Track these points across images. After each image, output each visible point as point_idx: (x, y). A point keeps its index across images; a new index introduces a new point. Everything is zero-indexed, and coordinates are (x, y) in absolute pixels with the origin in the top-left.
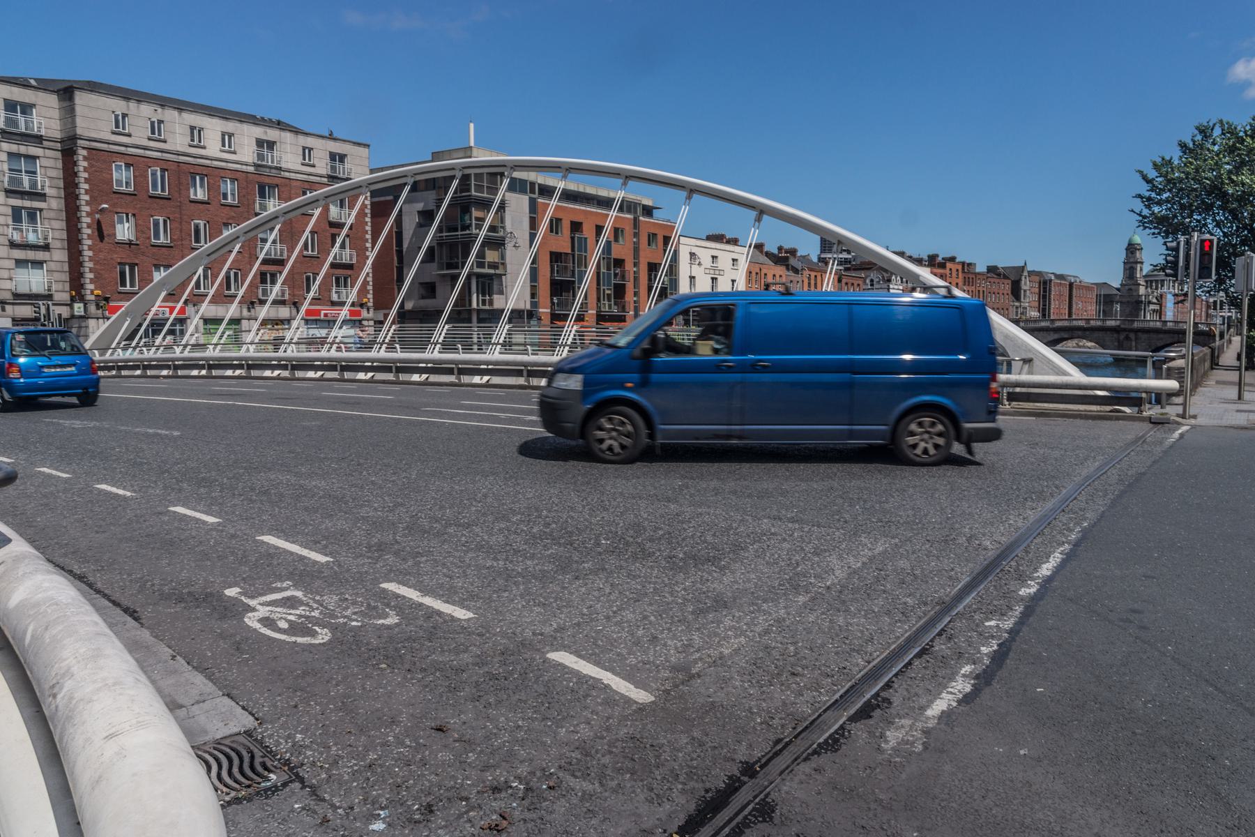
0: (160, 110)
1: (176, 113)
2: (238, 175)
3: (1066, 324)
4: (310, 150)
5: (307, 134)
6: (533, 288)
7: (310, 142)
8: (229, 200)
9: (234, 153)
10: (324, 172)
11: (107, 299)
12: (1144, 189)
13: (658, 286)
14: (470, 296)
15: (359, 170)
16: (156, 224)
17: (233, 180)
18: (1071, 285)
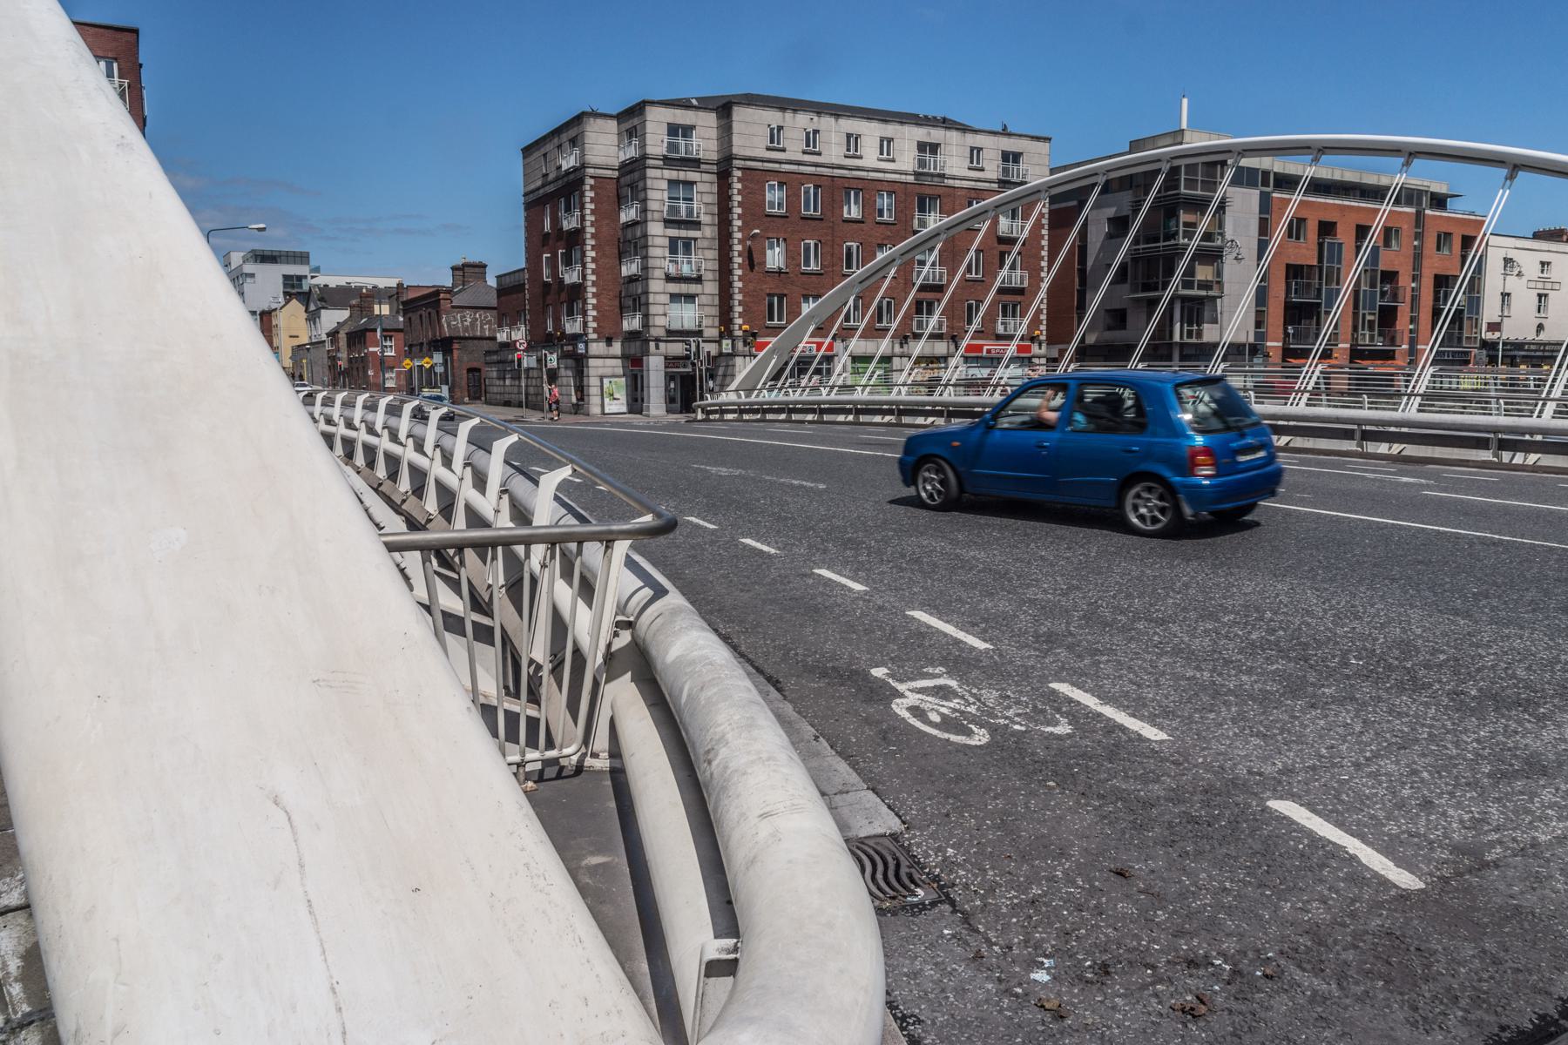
1: (832, 120)
2: (896, 187)
4: (980, 150)
9: (893, 161)
10: (994, 176)
11: (754, 335)
15: (1036, 171)
17: (890, 193)
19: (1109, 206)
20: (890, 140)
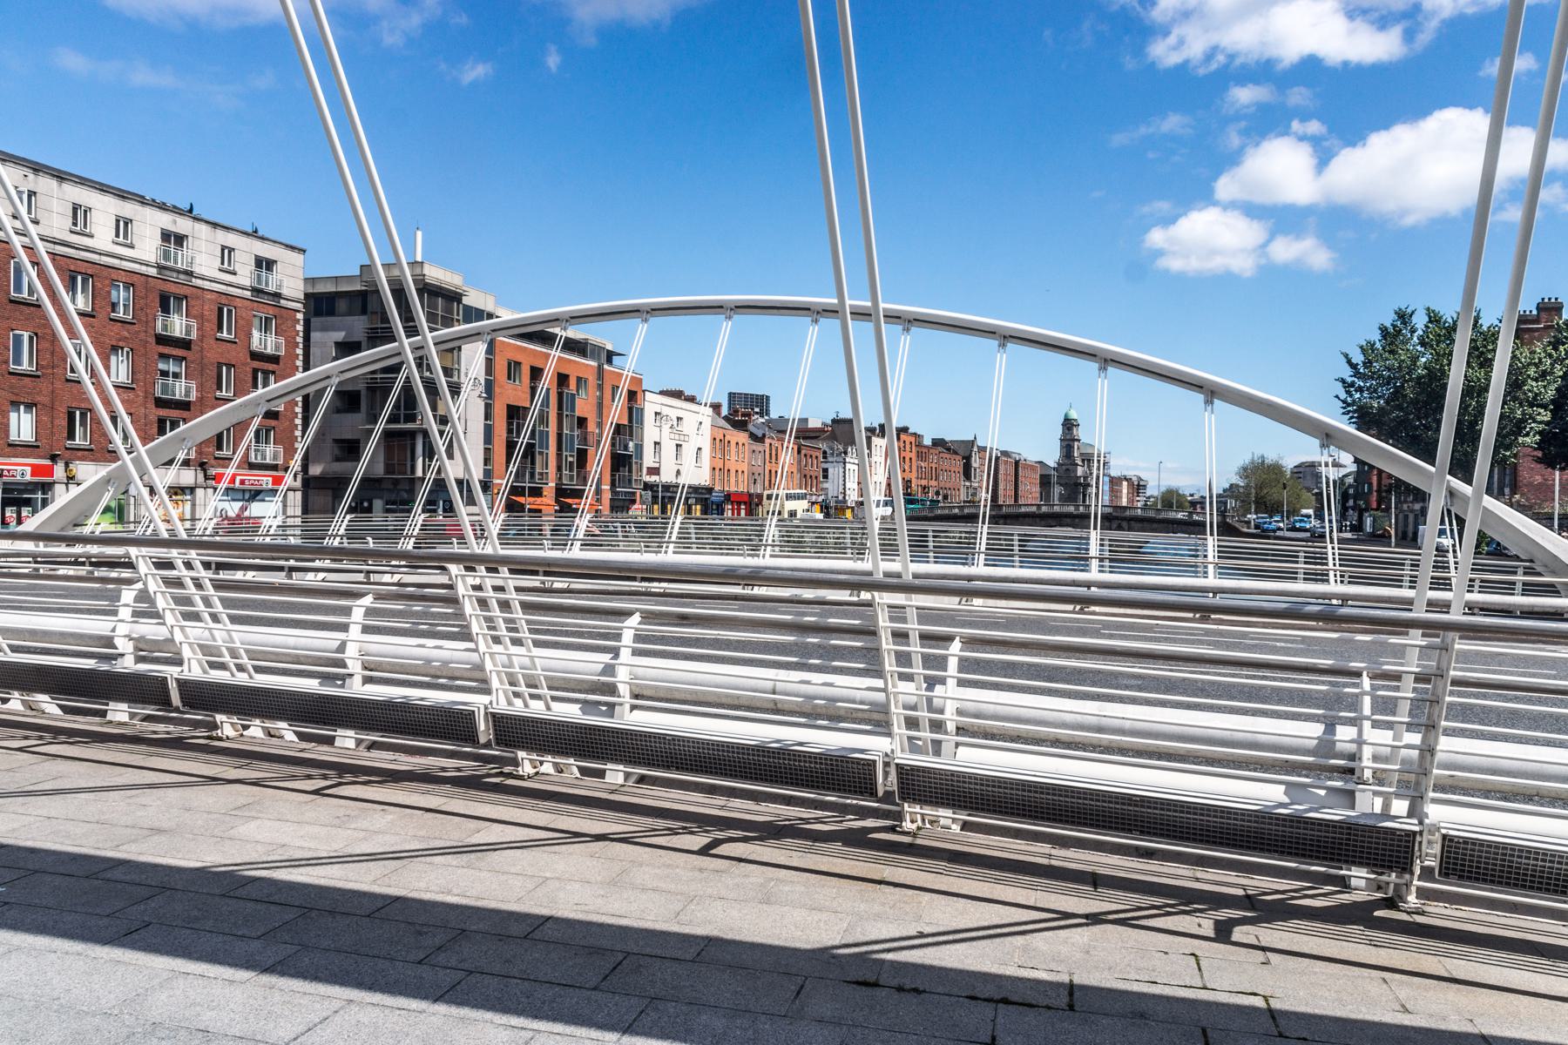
0: (31, 176)
2: (135, 279)
3: (1011, 510)
4: (231, 250)
5: (227, 228)
6: (487, 451)
7: (231, 239)
8: (121, 314)
9: (132, 247)
10: (247, 282)
12: (1347, 373)
13: (523, 440)
14: (413, 459)
15: (290, 281)
16: (18, 339)
17: (127, 286)
18: (1017, 463)
19: (339, 329)
20: (127, 222)
